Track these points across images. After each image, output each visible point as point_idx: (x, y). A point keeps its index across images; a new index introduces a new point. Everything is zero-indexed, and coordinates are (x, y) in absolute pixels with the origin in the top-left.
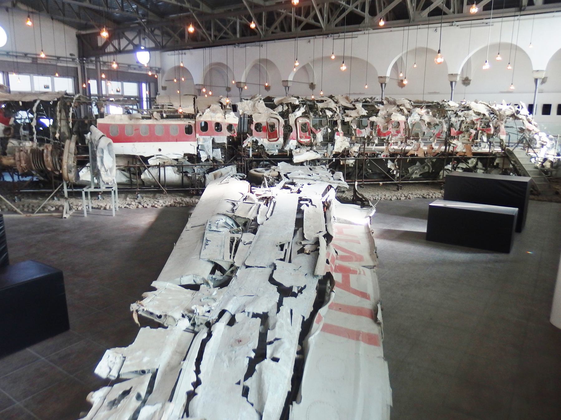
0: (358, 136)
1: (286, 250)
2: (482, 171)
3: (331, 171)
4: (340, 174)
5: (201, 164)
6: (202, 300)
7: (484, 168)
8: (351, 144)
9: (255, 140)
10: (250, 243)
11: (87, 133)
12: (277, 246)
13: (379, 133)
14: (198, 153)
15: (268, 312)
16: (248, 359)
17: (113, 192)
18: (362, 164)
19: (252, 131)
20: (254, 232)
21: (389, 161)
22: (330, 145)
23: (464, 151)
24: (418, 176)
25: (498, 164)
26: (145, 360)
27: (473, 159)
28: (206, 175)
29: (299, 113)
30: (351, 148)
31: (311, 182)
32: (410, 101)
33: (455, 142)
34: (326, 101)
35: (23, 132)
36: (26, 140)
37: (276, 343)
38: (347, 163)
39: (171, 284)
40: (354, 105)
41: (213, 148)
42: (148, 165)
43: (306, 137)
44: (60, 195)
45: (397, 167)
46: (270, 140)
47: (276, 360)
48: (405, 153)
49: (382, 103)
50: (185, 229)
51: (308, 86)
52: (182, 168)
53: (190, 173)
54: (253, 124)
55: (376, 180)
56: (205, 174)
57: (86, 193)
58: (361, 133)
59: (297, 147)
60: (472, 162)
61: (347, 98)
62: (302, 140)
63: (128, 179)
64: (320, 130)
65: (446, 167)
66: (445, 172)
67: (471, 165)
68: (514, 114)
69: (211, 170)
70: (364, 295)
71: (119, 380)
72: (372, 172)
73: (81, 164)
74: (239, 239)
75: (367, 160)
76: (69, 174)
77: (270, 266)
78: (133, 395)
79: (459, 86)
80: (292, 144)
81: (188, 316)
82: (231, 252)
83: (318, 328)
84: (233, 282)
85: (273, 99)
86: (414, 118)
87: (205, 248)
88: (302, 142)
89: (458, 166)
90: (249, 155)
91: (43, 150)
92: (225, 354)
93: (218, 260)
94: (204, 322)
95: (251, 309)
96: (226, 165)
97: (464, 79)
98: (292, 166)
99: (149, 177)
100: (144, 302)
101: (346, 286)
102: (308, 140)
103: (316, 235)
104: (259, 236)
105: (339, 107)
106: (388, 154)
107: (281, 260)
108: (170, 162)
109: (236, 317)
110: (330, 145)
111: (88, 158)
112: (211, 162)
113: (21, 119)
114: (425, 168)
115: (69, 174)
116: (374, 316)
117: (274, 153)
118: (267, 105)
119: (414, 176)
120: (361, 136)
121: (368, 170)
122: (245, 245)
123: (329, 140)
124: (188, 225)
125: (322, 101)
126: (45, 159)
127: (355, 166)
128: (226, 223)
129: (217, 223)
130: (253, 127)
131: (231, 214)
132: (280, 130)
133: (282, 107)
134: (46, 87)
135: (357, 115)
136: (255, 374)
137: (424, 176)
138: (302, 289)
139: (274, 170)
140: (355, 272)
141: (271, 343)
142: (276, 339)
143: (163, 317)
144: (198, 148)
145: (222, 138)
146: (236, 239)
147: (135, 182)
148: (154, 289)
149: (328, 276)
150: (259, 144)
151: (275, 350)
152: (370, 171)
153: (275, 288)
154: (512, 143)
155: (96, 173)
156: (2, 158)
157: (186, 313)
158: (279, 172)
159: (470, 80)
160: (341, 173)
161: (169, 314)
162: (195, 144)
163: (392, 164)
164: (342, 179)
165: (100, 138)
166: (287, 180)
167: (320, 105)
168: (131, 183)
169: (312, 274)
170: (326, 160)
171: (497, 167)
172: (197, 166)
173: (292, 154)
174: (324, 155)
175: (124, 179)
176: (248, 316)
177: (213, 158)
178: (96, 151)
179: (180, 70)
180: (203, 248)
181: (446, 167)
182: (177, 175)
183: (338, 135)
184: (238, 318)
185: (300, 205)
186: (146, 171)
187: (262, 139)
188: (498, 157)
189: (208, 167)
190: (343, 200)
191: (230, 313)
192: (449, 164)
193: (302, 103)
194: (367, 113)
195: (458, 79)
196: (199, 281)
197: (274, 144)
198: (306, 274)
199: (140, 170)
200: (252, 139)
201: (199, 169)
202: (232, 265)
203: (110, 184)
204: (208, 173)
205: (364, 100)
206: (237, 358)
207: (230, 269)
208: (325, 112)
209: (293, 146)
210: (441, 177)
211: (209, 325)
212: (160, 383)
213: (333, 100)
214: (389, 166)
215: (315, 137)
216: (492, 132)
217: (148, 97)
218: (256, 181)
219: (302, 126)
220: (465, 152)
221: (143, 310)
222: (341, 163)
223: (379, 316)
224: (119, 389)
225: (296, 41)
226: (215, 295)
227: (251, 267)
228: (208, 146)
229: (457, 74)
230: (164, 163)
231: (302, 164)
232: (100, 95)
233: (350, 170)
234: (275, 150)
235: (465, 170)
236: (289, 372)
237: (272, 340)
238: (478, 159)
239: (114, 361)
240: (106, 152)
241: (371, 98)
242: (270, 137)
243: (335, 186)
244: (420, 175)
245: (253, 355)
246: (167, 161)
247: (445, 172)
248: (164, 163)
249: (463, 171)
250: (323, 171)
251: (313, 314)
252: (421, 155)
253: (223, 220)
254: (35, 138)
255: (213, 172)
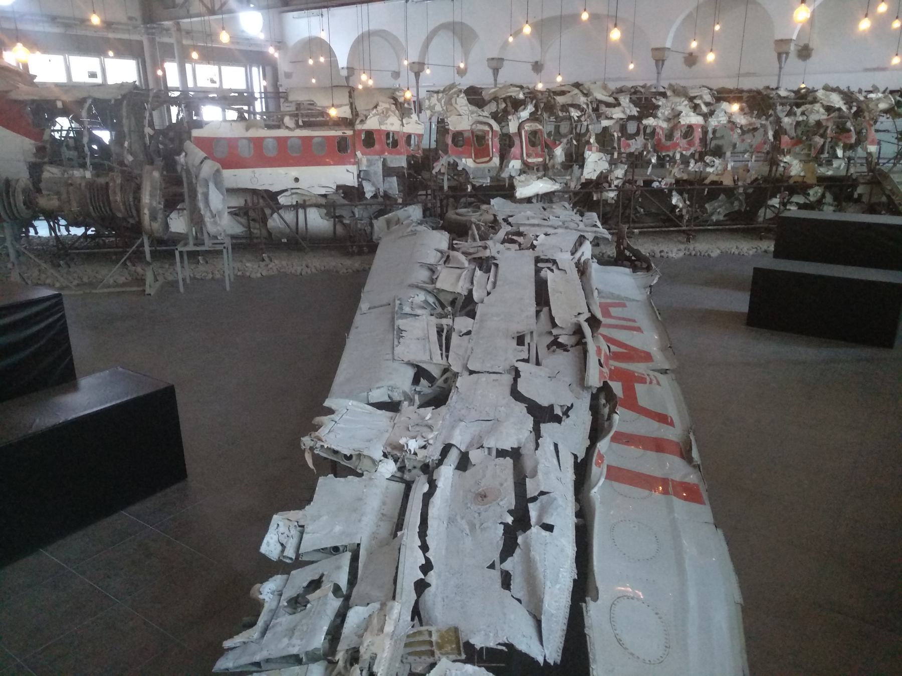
0: (623, 150)
1: (529, 344)
2: (832, 208)
3: (577, 211)
4: (593, 216)
5: (365, 202)
6: (410, 428)
7: (836, 203)
8: (610, 164)
9: (452, 162)
10: (469, 333)
11: (179, 154)
12: (513, 338)
13: (657, 148)
14: (360, 184)
15: (519, 448)
16: (502, 527)
17: (225, 251)
18: (630, 200)
19: (447, 145)
20: (472, 315)
21: (674, 193)
22: (576, 167)
23: (802, 174)
24: (721, 218)
25: (860, 196)
26: (338, 529)
27: (817, 188)
28: (374, 221)
29: (525, 114)
30: (610, 171)
31: (550, 231)
32: (711, 89)
33: (787, 159)
34: (569, 92)
35: (67, 154)
36: (73, 167)
37: (543, 498)
38: (604, 198)
39: (355, 403)
40: (616, 99)
41: (384, 176)
42: (278, 205)
43: (537, 156)
44: (139, 256)
45: (688, 203)
46: (478, 161)
47: (549, 528)
48: (700, 179)
49: (664, 95)
50: (358, 312)
51: (530, 67)
52: (334, 209)
53: (347, 218)
54: (448, 133)
55: (652, 224)
56: (371, 219)
57: (181, 253)
58: (629, 145)
59: (522, 172)
60: (815, 193)
61: (605, 87)
62: (530, 160)
63: (245, 229)
64: (561, 143)
65: (770, 202)
66: (768, 210)
67: (812, 199)
68: (894, 108)
69: (381, 213)
70: (663, 419)
71: (299, 563)
72: (644, 211)
73: (172, 203)
74: (450, 327)
75: (637, 193)
76: (152, 223)
77: (509, 372)
78: (327, 587)
79: (793, 62)
80: (515, 165)
81: (392, 456)
82: (441, 350)
83: (601, 474)
84: (453, 398)
85: (480, 91)
86: (718, 120)
87: (399, 343)
88: (529, 163)
89: (791, 200)
90: (442, 188)
91: (107, 184)
92: (462, 518)
93: (424, 362)
94: (419, 465)
95: (492, 443)
96: (405, 204)
97: (800, 48)
98: (514, 205)
99: (280, 226)
100: (322, 433)
101: (631, 403)
102: (540, 160)
103: (575, 320)
104: (482, 321)
105: (591, 102)
106: (674, 181)
107: (523, 360)
108: (314, 201)
109: (470, 456)
110: (576, 167)
111: (182, 195)
112: (380, 200)
113: (61, 130)
114: (735, 205)
115: (152, 223)
116: (686, 455)
117: (484, 183)
118: (471, 102)
119: (714, 218)
120: (628, 151)
121: (639, 209)
122: (460, 336)
123: (575, 159)
124: (364, 306)
125: (563, 93)
126: (111, 198)
127: (617, 202)
128: (426, 302)
129: (410, 301)
130: (449, 141)
131: (430, 287)
132: (494, 145)
133: (495, 103)
134: (93, 75)
135: (622, 116)
136: (518, 551)
137: (732, 217)
138: (569, 409)
139: (487, 212)
140: (642, 380)
141: (534, 499)
142: (542, 493)
143: (354, 458)
144: (359, 176)
145: (400, 161)
146: (445, 327)
147: (256, 234)
148: (330, 411)
149: (605, 388)
150: (460, 168)
151: (542, 512)
152: (642, 210)
153: (521, 408)
154: (884, 158)
155: (197, 220)
156: (37, 198)
157: (389, 449)
158: (495, 216)
159: (812, 50)
160: (595, 215)
161: (365, 453)
162: (354, 169)
163: (680, 197)
164: (599, 224)
165: (202, 162)
166: (509, 228)
167: (560, 100)
168: (250, 236)
169: (580, 384)
170: (569, 192)
171: (859, 200)
172: (360, 207)
173: (513, 183)
174: (566, 184)
175: (238, 229)
176: (490, 453)
177: (385, 192)
178: (196, 183)
179: (316, 45)
180: (396, 343)
181: (770, 202)
182: (326, 222)
183: (590, 150)
184: (475, 455)
185: (538, 271)
186: (275, 215)
187: (464, 160)
188: (863, 184)
189: (375, 208)
190: (604, 261)
191: (459, 449)
192: (776, 198)
193: (530, 97)
194: (637, 111)
195: (792, 47)
196: (397, 397)
197: (484, 168)
198: (570, 385)
199: (264, 214)
200: (448, 160)
201: (362, 212)
202: (446, 370)
203: (219, 238)
204: (376, 218)
205: (633, 90)
206: (485, 525)
207: (442, 376)
208: (567, 111)
209: (516, 170)
210: (761, 219)
211: (428, 469)
212: (365, 566)
213: (581, 91)
214: (674, 202)
215: (552, 156)
216: (853, 140)
217: (263, 91)
218: (458, 231)
219: (531, 137)
220: (804, 176)
221: (322, 446)
222: (595, 198)
223: (695, 454)
224: (301, 578)
225: (325, 18)
226: (430, 419)
227: (478, 372)
228: (375, 173)
229: (791, 40)
230: (304, 201)
231: (529, 200)
232: (185, 91)
233: (608, 209)
234: (485, 178)
235: (801, 207)
236: (570, 549)
237: (536, 494)
238: (826, 188)
239: (287, 532)
240: (212, 186)
241: (643, 87)
242: (477, 157)
243: (590, 236)
244: (725, 216)
245: (510, 520)
246: (310, 198)
247: (768, 210)
248: (304, 201)
249: (799, 209)
250: (564, 212)
251: (590, 450)
252: (728, 182)
253: (421, 297)
254: (88, 163)
255: (385, 216)
